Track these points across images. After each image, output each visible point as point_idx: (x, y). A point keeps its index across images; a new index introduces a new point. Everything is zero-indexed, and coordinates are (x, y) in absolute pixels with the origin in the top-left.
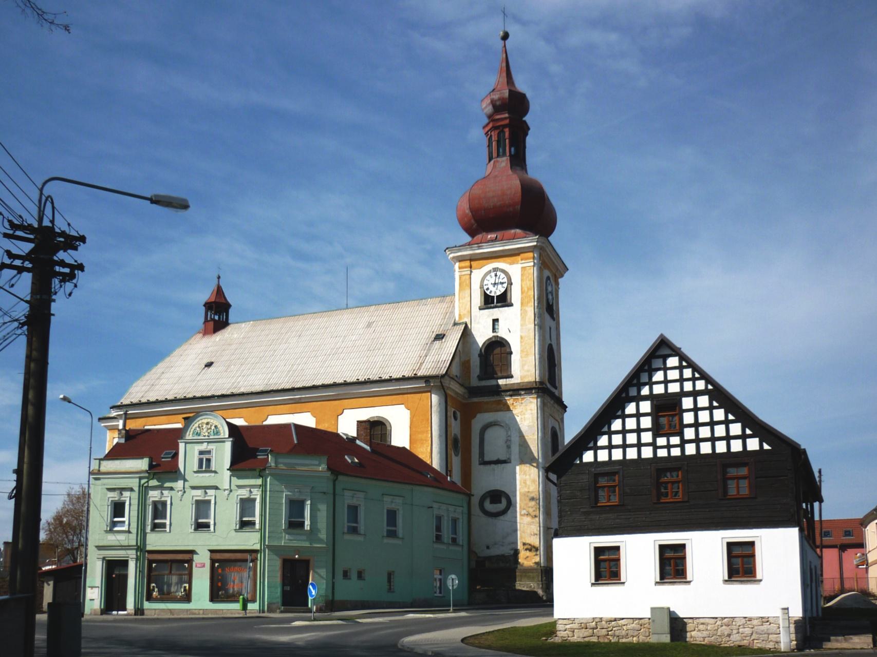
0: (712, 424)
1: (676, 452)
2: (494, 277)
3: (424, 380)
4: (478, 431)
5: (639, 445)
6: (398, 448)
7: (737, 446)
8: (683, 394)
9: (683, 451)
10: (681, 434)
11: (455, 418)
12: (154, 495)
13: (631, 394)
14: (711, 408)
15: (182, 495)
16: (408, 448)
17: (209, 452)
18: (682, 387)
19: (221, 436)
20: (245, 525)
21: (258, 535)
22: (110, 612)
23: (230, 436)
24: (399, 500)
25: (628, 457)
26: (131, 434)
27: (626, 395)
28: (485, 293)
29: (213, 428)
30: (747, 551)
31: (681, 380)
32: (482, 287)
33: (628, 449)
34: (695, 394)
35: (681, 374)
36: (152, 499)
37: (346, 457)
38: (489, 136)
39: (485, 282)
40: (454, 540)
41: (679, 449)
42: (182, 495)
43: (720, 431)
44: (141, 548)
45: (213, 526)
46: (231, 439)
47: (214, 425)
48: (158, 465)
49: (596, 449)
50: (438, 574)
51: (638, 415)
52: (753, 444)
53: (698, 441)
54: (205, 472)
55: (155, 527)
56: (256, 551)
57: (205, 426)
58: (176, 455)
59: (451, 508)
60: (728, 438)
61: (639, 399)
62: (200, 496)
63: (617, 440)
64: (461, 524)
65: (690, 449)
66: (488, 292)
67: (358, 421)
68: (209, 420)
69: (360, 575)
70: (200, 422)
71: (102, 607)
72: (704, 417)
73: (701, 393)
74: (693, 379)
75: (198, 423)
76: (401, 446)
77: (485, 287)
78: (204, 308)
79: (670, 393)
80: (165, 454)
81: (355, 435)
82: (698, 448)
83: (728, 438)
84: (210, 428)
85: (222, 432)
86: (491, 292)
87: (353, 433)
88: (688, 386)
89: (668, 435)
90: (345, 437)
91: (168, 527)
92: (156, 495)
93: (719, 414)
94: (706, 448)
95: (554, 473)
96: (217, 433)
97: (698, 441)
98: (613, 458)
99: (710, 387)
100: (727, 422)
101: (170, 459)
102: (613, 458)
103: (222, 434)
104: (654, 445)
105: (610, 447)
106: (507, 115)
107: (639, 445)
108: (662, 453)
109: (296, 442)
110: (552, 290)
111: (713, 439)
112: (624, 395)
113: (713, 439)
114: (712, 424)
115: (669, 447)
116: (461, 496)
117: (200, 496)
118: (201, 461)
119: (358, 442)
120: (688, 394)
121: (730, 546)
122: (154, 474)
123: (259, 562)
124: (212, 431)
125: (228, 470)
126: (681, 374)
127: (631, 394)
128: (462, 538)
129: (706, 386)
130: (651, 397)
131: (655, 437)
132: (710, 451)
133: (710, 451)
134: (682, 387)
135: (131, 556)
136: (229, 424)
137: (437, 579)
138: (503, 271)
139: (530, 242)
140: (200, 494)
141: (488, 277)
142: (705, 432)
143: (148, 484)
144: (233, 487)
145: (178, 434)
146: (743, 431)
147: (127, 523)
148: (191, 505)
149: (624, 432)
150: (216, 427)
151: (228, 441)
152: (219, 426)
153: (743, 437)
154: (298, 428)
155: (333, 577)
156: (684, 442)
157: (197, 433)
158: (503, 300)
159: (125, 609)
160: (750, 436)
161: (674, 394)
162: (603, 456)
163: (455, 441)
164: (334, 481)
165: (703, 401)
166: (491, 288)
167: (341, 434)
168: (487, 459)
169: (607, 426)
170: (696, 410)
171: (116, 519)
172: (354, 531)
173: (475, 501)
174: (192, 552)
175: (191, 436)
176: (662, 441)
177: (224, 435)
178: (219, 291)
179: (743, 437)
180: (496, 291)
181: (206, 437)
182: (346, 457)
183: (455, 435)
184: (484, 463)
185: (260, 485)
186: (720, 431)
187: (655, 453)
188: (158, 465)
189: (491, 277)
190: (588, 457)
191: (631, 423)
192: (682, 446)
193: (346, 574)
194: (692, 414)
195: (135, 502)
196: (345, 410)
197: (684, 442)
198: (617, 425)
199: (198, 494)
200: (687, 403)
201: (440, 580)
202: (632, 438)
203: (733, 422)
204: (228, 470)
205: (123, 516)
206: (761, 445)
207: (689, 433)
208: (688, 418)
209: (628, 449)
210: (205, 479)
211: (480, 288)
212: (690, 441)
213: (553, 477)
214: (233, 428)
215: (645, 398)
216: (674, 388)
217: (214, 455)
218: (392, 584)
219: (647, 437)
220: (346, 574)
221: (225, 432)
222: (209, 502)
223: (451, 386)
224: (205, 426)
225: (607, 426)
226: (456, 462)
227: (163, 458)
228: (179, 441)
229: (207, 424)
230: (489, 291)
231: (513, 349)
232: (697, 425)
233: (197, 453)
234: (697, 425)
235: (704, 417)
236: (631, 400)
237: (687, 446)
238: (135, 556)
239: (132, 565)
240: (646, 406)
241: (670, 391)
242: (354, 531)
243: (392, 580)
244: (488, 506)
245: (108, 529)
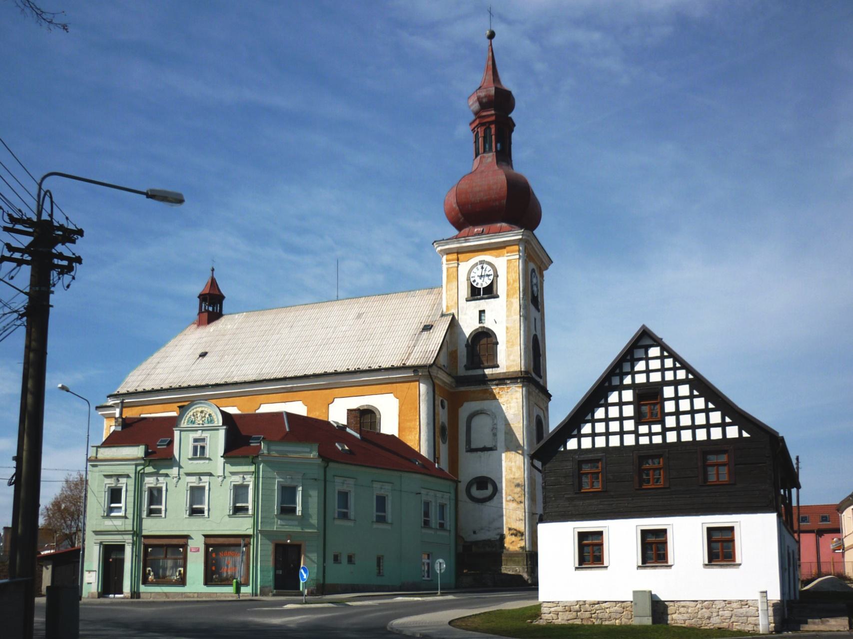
0: (693, 412)
1: (657, 440)
2: (481, 270)
4: (465, 420)
5: (622, 433)
6: (388, 436)
7: (716, 434)
8: (664, 383)
9: (664, 438)
10: (662, 422)
11: (443, 407)
12: (150, 482)
13: (614, 383)
14: (691, 397)
15: (177, 482)
16: (397, 435)
17: (203, 440)
18: (663, 376)
19: (215, 424)
20: (238, 510)
21: (251, 521)
22: (107, 596)
23: (224, 424)
24: (388, 487)
25: (611, 444)
26: (127, 422)
27: (609, 384)
28: (472, 285)
29: (207, 416)
30: (726, 536)
31: (663, 370)
32: (468, 279)
33: (611, 437)
34: (676, 383)
35: (663, 364)
36: (148, 486)
37: (337, 444)
38: (475, 132)
39: (472, 275)
40: (442, 526)
41: (660, 437)
42: (177, 482)
43: (700, 419)
44: (137, 533)
45: (207, 511)
46: (225, 427)
47: (208, 414)
48: (154, 452)
49: (580, 436)
50: (426, 558)
51: (621, 404)
52: (733, 432)
53: (678, 429)
54: (200, 459)
55: (151, 512)
56: (249, 536)
57: (199, 414)
58: (171, 443)
60: (708, 426)
61: (621, 388)
62: (194, 482)
63: (600, 427)
64: (448, 510)
65: (671, 437)
66: (474, 284)
67: (348, 410)
68: (203, 409)
69: (350, 559)
70: (195, 410)
71: (100, 590)
72: (685, 405)
73: (682, 382)
74: (674, 369)
75: (192, 412)
76: (390, 433)
77: (472, 280)
78: (198, 300)
79: (651, 382)
80: (161, 442)
81: (345, 423)
82: (679, 436)
83: (708, 426)
84: (205, 417)
85: (216, 420)
86: (477, 284)
87: (344, 421)
88: (669, 376)
89: (650, 423)
90: (335, 425)
91: (163, 512)
92: (152, 482)
93: (699, 403)
94: (686, 436)
95: (539, 460)
96: (211, 421)
97: (678, 429)
98: (597, 446)
99: (691, 376)
100: (707, 411)
101: (165, 447)
102: (597, 446)
103: (216, 422)
104: (636, 432)
105: (594, 435)
106: (493, 112)
107: (622, 433)
108: (644, 441)
109: (288, 430)
111: (693, 427)
112: (607, 384)
113: (693, 427)
114: (693, 412)
115: (650, 434)
116: (448, 483)
117: (194, 482)
118: (195, 448)
119: (348, 430)
120: (669, 383)
121: (710, 531)
122: (150, 461)
123: (252, 547)
124: (206, 419)
125: (222, 457)
126: (663, 364)
127: (614, 383)
128: (449, 523)
129: (687, 376)
130: (633, 386)
131: (637, 425)
132: (690, 439)
133: (690, 439)
134: (663, 376)
135: (127, 541)
136: (223, 413)
137: (425, 564)
139: (516, 235)
140: (194, 481)
141: (475, 270)
142: (685, 420)
143: (144, 471)
144: (227, 474)
145: (173, 422)
146: (723, 419)
147: (123, 509)
148: (186, 491)
149: (607, 420)
150: (210, 415)
151: (221, 429)
152: (213, 415)
153: (723, 425)
154: (290, 416)
155: (324, 561)
156: (665, 430)
158: (490, 292)
159: (121, 593)
160: (730, 424)
161: (656, 384)
162: (586, 443)
163: (443, 429)
164: (325, 468)
165: (684, 390)
166: (478, 280)
167: (332, 422)
168: (473, 446)
169: (590, 414)
170: (677, 398)
171: (113, 505)
172: (344, 516)
173: (462, 487)
175: (186, 424)
176: (643, 429)
177: (218, 423)
178: (213, 283)
179: (723, 425)
180: (483, 283)
181: (201, 426)
182: (337, 444)
183: (443, 423)
184: (471, 450)
185: (253, 472)
186: (700, 419)
187: (637, 440)
189: (478, 270)
190: (572, 444)
191: (614, 412)
192: (663, 433)
193: (336, 559)
194: (673, 403)
195: (131, 488)
197: (665, 430)
198: (600, 413)
199: (193, 481)
200: (668, 392)
201: (428, 564)
202: (614, 426)
203: (713, 410)
204: (222, 457)
205: (120, 502)
206: (740, 433)
207: (670, 422)
208: (669, 407)
209: (611, 437)
210: (200, 466)
211: (467, 280)
212: (671, 429)
213: (538, 464)
214: (226, 417)
215: (627, 387)
216: (655, 377)
217: (208, 443)
218: (381, 568)
219: (629, 425)
220: (336, 559)
221: (219, 420)
223: (438, 376)
224: (199, 414)
225: (590, 414)
226: (444, 449)
227: (158, 445)
228: (174, 429)
230: (476, 283)
231: (499, 340)
232: (677, 413)
233: (191, 441)
234: (677, 413)
235: (685, 405)
236: (614, 389)
237: (668, 434)
238: (131, 541)
239: (128, 550)
240: (628, 395)
241: (652, 380)
242: (344, 516)
243: (381, 564)
244: (475, 492)
245: (105, 514)
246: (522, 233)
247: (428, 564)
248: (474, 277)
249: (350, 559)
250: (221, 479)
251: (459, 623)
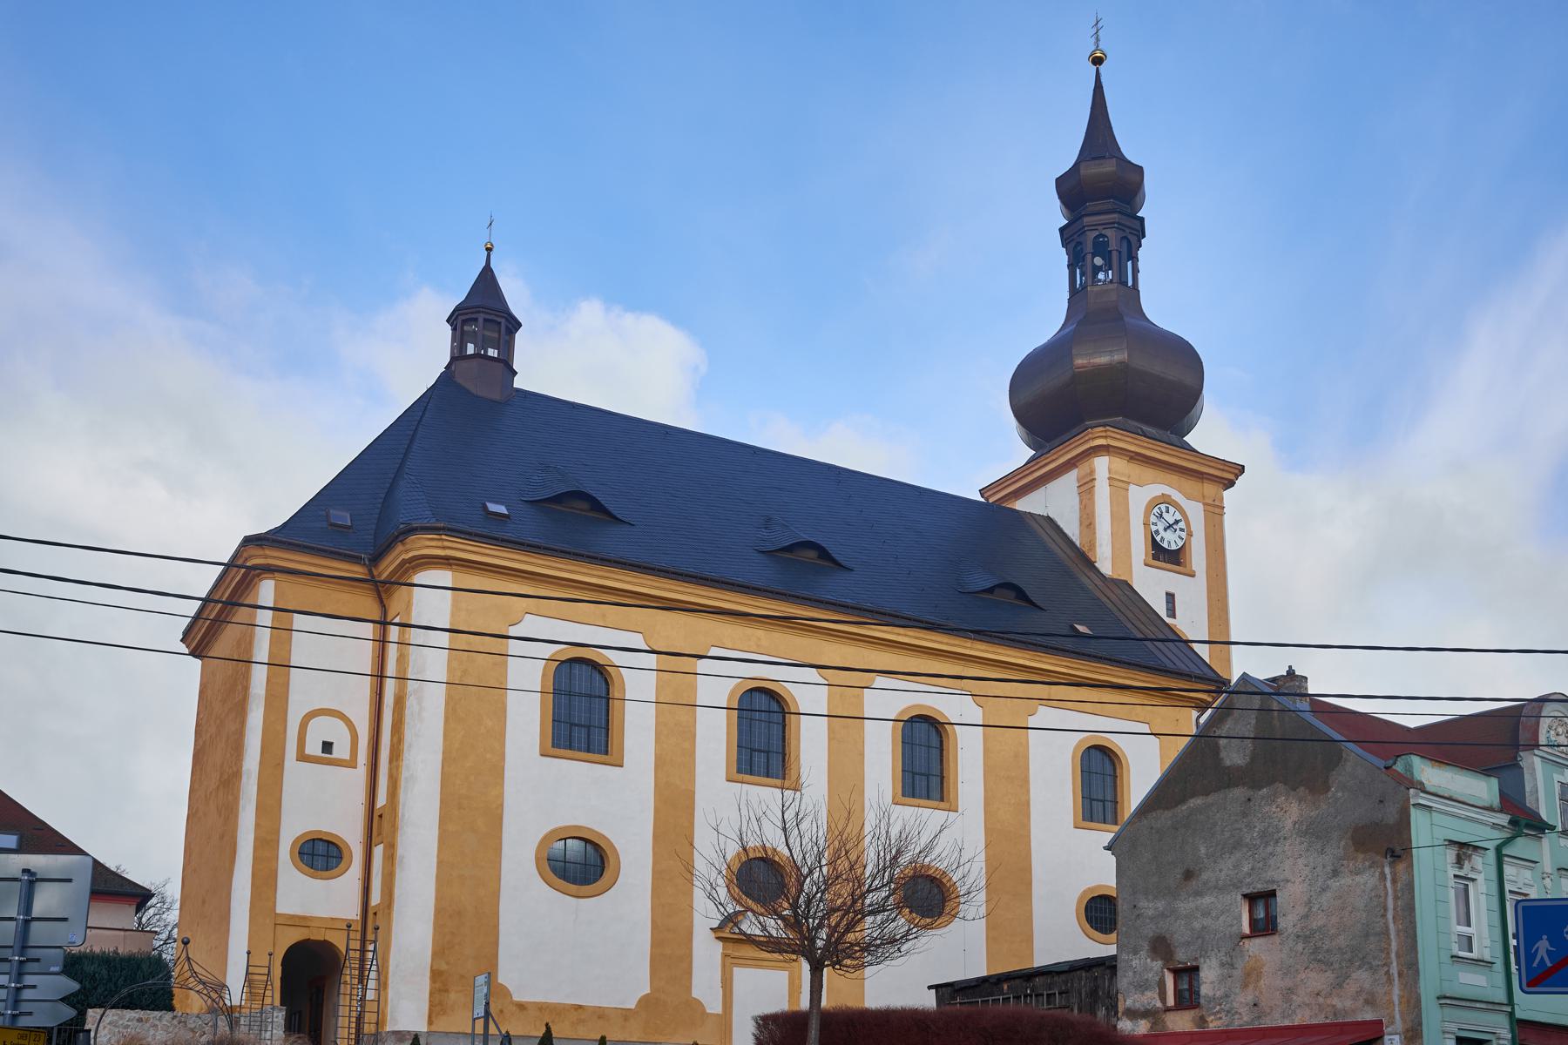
32: (1146, 524)
66: (1158, 539)
77: (1154, 528)
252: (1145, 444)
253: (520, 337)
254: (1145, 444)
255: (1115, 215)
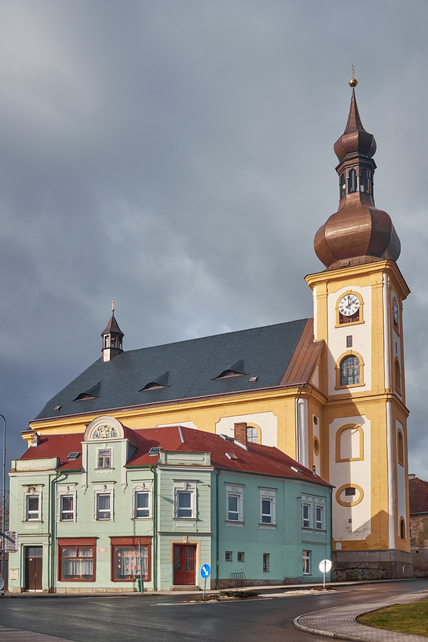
2: (347, 300)
3: (127, 565)
11: (316, 423)
12: (61, 490)
15: (86, 490)
16: (276, 447)
17: (108, 451)
20: (138, 514)
21: (151, 523)
22: (27, 590)
23: (125, 438)
24: (273, 494)
26: (41, 438)
36: (60, 494)
37: (227, 454)
38: (341, 174)
42: (86, 490)
44: (52, 535)
45: (113, 516)
46: (127, 440)
47: (111, 428)
48: (65, 463)
50: (306, 555)
54: (105, 468)
55: (63, 517)
57: (103, 429)
59: (317, 500)
70: (99, 426)
71: (22, 586)
77: (340, 309)
80: (71, 455)
81: (233, 437)
85: (118, 434)
86: (346, 312)
87: (231, 435)
90: (224, 438)
91: (74, 517)
92: (64, 490)
96: (115, 435)
101: (75, 459)
103: (119, 436)
106: (357, 152)
109: (183, 441)
110: (397, 311)
118: (101, 459)
119: (236, 442)
123: (152, 546)
124: (110, 433)
125: (124, 467)
128: (323, 521)
135: (44, 543)
136: (124, 427)
137: (305, 560)
138: (356, 294)
139: (382, 265)
143: (57, 480)
145: (81, 437)
147: (40, 515)
148: (94, 498)
150: (113, 429)
155: (218, 560)
157: (97, 435)
158: (355, 317)
159: (41, 588)
163: (316, 442)
164: (217, 475)
166: (346, 310)
167: (221, 436)
168: (342, 457)
171: (30, 512)
174: (97, 538)
175: (92, 437)
177: (120, 436)
180: (352, 311)
181: (105, 439)
182: (227, 454)
183: (315, 437)
185: (153, 480)
188: (65, 463)
189: (345, 300)
193: (228, 556)
195: (46, 496)
196: (221, 418)
199: (99, 489)
201: (307, 560)
204: (124, 467)
205: (38, 510)
210: (105, 474)
214: (128, 432)
218: (267, 565)
220: (228, 556)
221: (121, 433)
222: (229, 559)
223: (312, 395)
224: (103, 429)
226: (317, 460)
227: (68, 458)
228: (82, 443)
229: (105, 426)
230: (344, 312)
233: (97, 453)
238: (48, 543)
239: (45, 550)
242: (266, 496)
243: (267, 561)
245: (25, 520)
246: (385, 263)
247: (307, 560)
248: (342, 307)
249: (240, 556)
250: (124, 487)
251: (364, 618)
252: (330, 274)
253: (124, 339)
254: (330, 274)
255: (358, 159)
